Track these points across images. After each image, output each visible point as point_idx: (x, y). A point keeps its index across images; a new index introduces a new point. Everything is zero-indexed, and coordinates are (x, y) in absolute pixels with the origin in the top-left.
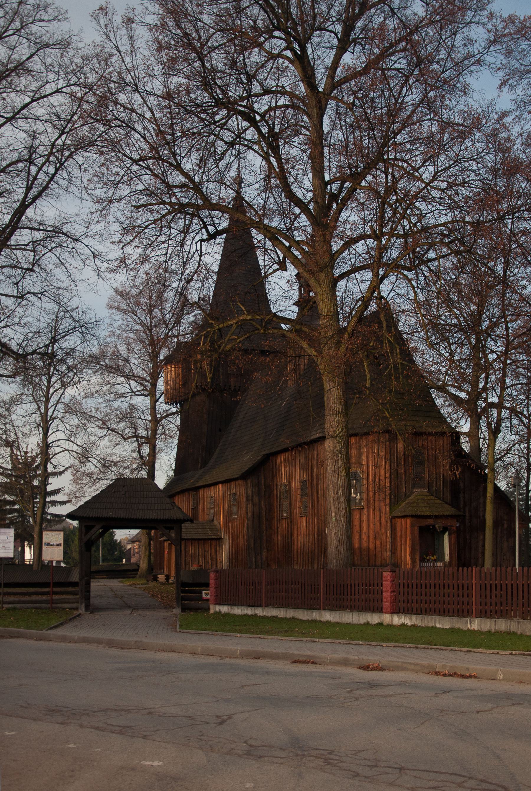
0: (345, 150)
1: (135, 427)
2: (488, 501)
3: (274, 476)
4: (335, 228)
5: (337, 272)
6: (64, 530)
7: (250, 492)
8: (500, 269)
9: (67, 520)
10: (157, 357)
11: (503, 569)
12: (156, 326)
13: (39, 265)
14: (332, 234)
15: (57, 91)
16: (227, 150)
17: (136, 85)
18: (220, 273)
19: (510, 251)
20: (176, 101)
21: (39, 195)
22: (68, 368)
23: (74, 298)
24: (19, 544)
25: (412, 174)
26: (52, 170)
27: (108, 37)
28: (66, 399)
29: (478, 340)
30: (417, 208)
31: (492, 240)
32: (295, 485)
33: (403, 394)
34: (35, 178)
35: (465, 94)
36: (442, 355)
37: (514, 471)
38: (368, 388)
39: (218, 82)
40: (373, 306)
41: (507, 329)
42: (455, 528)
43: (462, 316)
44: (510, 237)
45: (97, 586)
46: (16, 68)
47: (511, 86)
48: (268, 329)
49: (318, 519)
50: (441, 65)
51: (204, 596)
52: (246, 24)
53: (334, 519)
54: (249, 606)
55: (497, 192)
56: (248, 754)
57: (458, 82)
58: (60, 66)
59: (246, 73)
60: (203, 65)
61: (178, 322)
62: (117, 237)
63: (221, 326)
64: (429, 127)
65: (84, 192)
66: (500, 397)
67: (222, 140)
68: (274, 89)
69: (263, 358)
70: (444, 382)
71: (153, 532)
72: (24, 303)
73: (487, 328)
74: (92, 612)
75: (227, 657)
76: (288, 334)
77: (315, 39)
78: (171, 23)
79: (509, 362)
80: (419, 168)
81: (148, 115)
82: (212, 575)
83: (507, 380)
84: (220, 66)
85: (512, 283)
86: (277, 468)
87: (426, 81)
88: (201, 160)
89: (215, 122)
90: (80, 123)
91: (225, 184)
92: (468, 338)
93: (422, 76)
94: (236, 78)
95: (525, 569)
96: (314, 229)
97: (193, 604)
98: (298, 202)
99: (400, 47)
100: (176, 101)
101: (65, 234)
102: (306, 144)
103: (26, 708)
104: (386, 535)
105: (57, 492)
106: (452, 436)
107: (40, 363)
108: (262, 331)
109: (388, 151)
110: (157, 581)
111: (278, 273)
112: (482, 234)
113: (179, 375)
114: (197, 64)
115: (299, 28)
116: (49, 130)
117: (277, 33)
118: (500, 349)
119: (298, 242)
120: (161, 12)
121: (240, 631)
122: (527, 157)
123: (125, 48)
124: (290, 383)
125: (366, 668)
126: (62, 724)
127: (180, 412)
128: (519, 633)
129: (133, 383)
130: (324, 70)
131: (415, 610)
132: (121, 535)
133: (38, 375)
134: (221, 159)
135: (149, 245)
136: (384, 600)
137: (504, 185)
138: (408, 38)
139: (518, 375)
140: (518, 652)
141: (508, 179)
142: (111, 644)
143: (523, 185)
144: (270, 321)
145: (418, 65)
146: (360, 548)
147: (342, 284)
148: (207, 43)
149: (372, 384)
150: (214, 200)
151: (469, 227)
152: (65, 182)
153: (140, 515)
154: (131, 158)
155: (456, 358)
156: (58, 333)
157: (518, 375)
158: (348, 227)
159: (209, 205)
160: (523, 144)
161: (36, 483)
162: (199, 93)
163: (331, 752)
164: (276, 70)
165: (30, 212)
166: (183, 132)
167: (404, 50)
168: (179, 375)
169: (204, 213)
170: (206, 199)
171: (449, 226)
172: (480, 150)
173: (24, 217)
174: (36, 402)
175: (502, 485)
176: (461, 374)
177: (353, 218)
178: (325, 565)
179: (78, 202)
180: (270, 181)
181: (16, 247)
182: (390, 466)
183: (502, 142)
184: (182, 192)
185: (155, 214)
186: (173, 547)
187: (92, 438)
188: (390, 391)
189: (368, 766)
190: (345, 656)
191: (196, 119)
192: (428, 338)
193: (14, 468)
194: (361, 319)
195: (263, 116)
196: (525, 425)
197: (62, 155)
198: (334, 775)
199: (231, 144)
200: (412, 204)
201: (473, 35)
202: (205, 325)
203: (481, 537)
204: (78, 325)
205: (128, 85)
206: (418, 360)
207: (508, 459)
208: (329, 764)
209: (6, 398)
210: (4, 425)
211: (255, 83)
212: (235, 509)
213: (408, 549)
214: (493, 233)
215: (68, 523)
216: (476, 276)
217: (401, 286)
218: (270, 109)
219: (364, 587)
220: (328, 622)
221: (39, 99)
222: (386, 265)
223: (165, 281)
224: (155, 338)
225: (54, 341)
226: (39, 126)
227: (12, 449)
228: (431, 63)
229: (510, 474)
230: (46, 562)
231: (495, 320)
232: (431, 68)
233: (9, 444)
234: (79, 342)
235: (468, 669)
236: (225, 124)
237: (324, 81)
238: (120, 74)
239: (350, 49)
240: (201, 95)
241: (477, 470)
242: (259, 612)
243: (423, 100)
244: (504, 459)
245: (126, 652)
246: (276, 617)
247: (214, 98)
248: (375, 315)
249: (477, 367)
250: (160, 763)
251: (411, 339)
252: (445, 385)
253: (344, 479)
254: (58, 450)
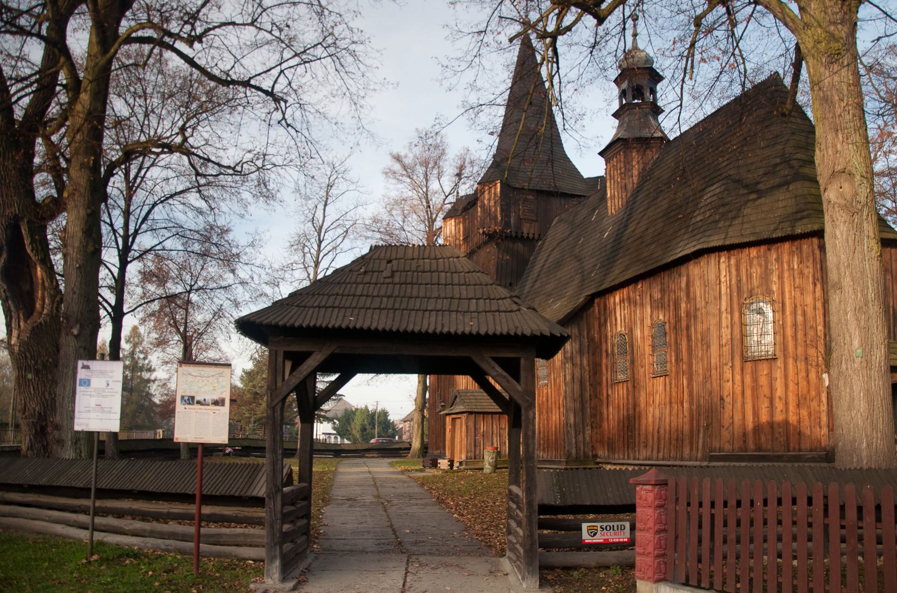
3: (602, 325)
49: (690, 380)
51: (586, 537)
86: (606, 314)
104: (820, 401)
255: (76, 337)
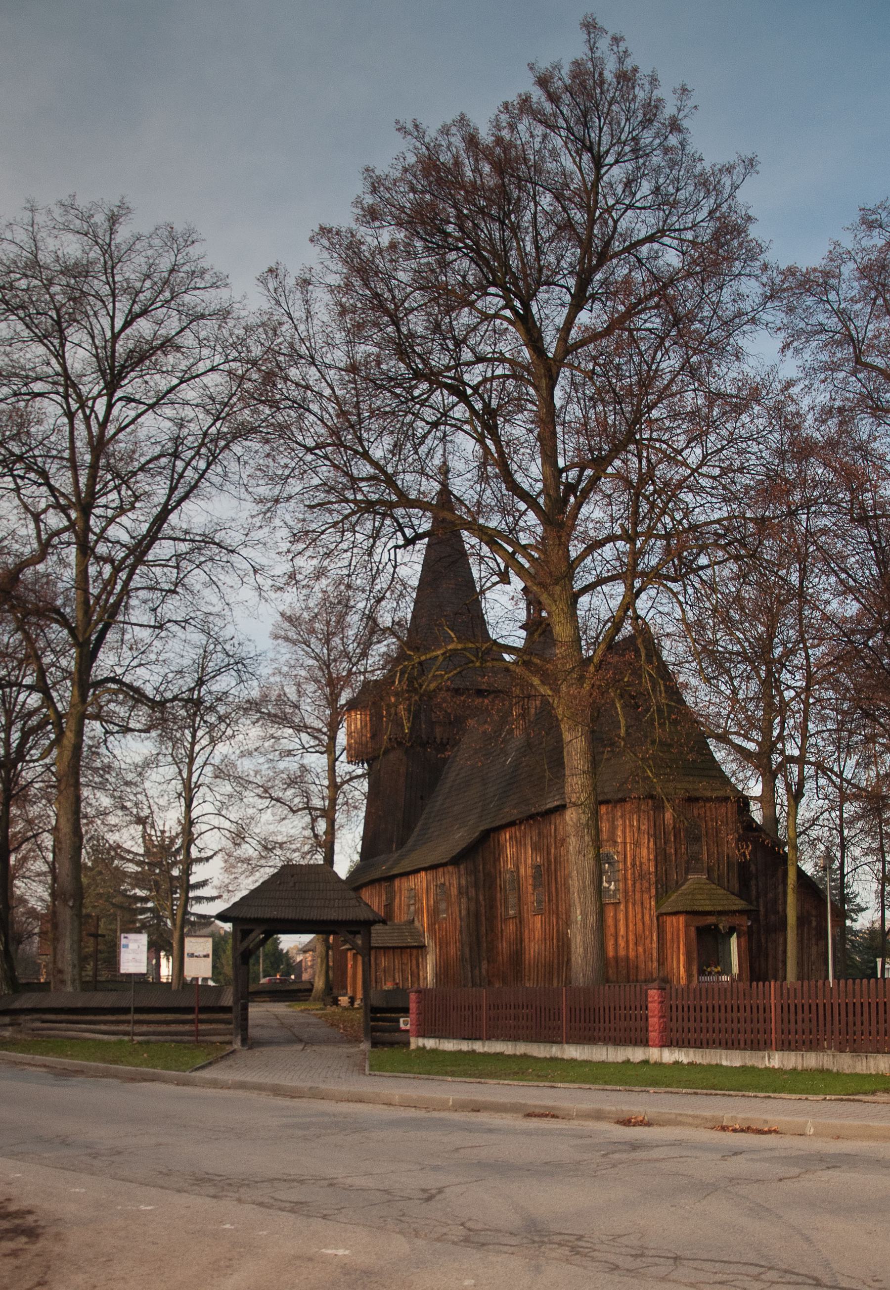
0: (584, 429)
1: (307, 795)
2: (790, 891)
3: (497, 860)
4: (573, 527)
5: (577, 586)
6: (212, 935)
7: (463, 882)
8: (794, 578)
9: (218, 922)
10: (336, 701)
11: (813, 983)
12: (335, 660)
13: (183, 585)
14: (569, 535)
15: (213, 369)
16: (429, 432)
17: (312, 357)
18: (420, 589)
19: (807, 555)
20: (363, 374)
21: (186, 497)
22: (220, 717)
23: (228, 626)
24: (153, 955)
25: (673, 458)
26: (202, 465)
27: (278, 303)
28: (216, 760)
29: (769, 672)
30: (681, 500)
31: (782, 541)
32: (526, 871)
33: (670, 746)
34: (181, 476)
35: (738, 358)
36: (721, 692)
37: (823, 848)
38: (623, 739)
39: (418, 349)
40: (627, 629)
41: (807, 657)
42: (745, 928)
43: (747, 640)
44: (806, 536)
45: (257, 1011)
46: (162, 345)
47: (796, 350)
48: (487, 661)
49: (558, 918)
50: (705, 325)
51: (402, 1026)
52: (453, 279)
53: (579, 918)
54: (464, 1039)
55: (787, 480)
56: (467, 1240)
57: (728, 344)
58: (217, 339)
59: (454, 338)
60: (398, 330)
61: (364, 655)
62: (284, 546)
63: (423, 658)
64: (692, 399)
65: (243, 490)
66: (802, 748)
67: (423, 420)
68: (489, 356)
69: (481, 700)
70: (725, 728)
71: (331, 937)
72: (163, 634)
73: (781, 657)
74: (250, 1048)
75: (434, 1110)
76: (512, 667)
77: (542, 296)
78: (357, 282)
79: (811, 701)
80: (682, 450)
81: (327, 392)
82: (413, 996)
83: (811, 726)
84: (420, 330)
85: (811, 596)
86: (500, 848)
87: (686, 343)
88: (395, 446)
89: (413, 398)
90: (240, 405)
91: (427, 475)
92: (756, 669)
93: (682, 337)
94: (441, 344)
95: (842, 982)
96: (545, 530)
97: (387, 1036)
98: (524, 496)
99: (652, 303)
100: (363, 374)
101: (218, 544)
102: (532, 422)
103: (166, 1175)
104: (652, 939)
105: (203, 884)
106: (738, 801)
107: (183, 713)
108: (478, 664)
109: (641, 430)
110: (337, 1005)
111: (498, 586)
112: (769, 534)
113: (366, 725)
114: (390, 329)
115: (521, 283)
116: (201, 416)
117: (492, 290)
118: (798, 684)
119: (525, 547)
120: (345, 271)
121: (452, 1074)
122: (823, 436)
123: (298, 313)
124: (517, 733)
125: (627, 1122)
126: (214, 1197)
127: (368, 774)
128: (835, 1070)
129: (304, 736)
130: (554, 332)
131: (692, 1042)
132: (289, 942)
133: (180, 728)
134: (420, 444)
135: (327, 555)
136: (650, 1029)
137: (794, 472)
138: (660, 292)
139: (824, 719)
140: (833, 1097)
141: (799, 463)
142: (277, 1091)
143: (820, 471)
144: (488, 651)
145: (675, 324)
146: (616, 958)
147: (584, 600)
148: (402, 304)
149: (628, 734)
150: (413, 495)
151: (751, 525)
152: (219, 478)
153: (314, 915)
154: (304, 446)
155: (740, 697)
156: (205, 672)
157: (824, 719)
158: (591, 525)
159: (405, 501)
160: (816, 420)
161: (175, 872)
162: (392, 363)
163: (580, 1238)
164: (492, 333)
165: (173, 518)
166: (372, 412)
167: (657, 306)
168: (366, 725)
169: (399, 512)
170: (402, 494)
171: (725, 523)
172: (761, 428)
173: (165, 525)
174: (177, 764)
175: (808, 868)
176: (747, 718)
177: (598, 514)
178: (568, 980)
179: (235, 502)
180: (486, 469)
181: (155, 563)
182: (655, 843)
183: (789, 417)
184: (370, 486)
185: (335, 514)
186: (360, 958)
187: (251, 811)
188: (653, 742)
189: (632, 1256)
190: (598, 1106)
191: (388, 394)
192: (702, 670)
193: (147, 852)
194: (611, 646)
195: (476, 389)
196: (835, 786)
197: (216, 446)
198: (585, 1268)
199: (435, 425)
200: (676, 496)
201: (743, 289)
202: (402, 657)
203: (781, 940)
204: (232, 661)
205: (301, 357)
206: (689, 700)
207: (814, 833)
208: (578, 1253)
209: (139, 760)
210: (135, 795)
211: (465, 349)
212: (443, 906)
213: (682, 957)
214: (783, 532)
215: (217, 926)
216: (763, 588)
217: (664, 601)
218: (485, 380)
219: (623, 1012)
220: (573, 1061)
221: (189, 380)
222: (643, 574)
223: (348, 600)
224: (334, 676)
225: (200, 682)
226: (188, 412)
227: (144, 828)
228: (692, 322)
229: (818, 853)
230: (189, 979)
231: (790, 645)
232: (693, 327)
233: (141, 821)
234: (234, 683)
235: (766, 1122)
236: (426, 400)
237: (555, 344)
238: (291, 345)
239: (588, 306)
240: (394, 366)
241: (773, 848)
242: (479, 1047)
243: (684, 365)
244: (809, 832)
245: (296, 1103)
246: (502, 1054)
247: (412, 369)
248: (631, 639)
249: (770, 708)
250: (347, 1252)
251: (679, 672)
252: (727, 732)
253: (592, 862)
254: (204, 827)
255: (72, 908)
